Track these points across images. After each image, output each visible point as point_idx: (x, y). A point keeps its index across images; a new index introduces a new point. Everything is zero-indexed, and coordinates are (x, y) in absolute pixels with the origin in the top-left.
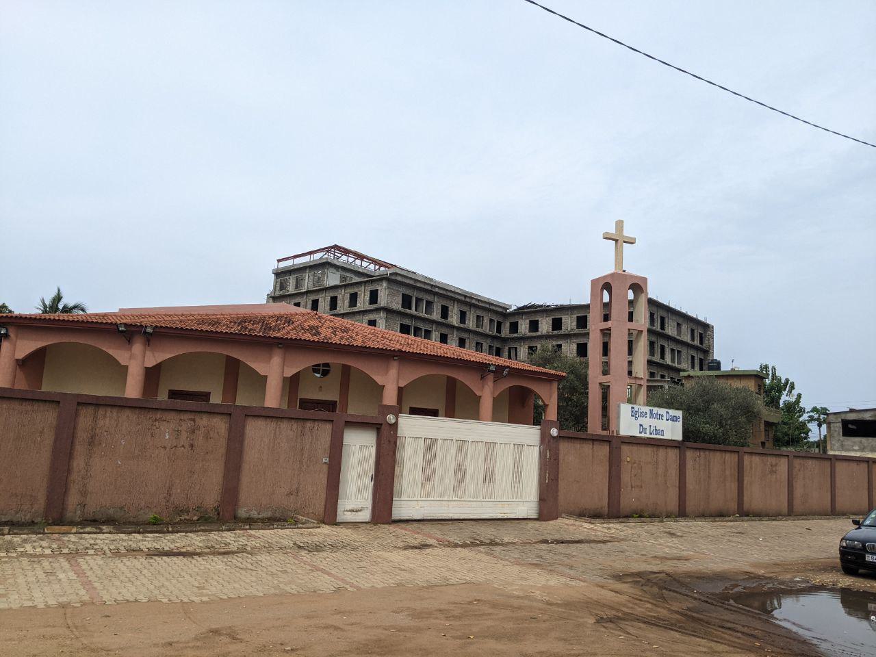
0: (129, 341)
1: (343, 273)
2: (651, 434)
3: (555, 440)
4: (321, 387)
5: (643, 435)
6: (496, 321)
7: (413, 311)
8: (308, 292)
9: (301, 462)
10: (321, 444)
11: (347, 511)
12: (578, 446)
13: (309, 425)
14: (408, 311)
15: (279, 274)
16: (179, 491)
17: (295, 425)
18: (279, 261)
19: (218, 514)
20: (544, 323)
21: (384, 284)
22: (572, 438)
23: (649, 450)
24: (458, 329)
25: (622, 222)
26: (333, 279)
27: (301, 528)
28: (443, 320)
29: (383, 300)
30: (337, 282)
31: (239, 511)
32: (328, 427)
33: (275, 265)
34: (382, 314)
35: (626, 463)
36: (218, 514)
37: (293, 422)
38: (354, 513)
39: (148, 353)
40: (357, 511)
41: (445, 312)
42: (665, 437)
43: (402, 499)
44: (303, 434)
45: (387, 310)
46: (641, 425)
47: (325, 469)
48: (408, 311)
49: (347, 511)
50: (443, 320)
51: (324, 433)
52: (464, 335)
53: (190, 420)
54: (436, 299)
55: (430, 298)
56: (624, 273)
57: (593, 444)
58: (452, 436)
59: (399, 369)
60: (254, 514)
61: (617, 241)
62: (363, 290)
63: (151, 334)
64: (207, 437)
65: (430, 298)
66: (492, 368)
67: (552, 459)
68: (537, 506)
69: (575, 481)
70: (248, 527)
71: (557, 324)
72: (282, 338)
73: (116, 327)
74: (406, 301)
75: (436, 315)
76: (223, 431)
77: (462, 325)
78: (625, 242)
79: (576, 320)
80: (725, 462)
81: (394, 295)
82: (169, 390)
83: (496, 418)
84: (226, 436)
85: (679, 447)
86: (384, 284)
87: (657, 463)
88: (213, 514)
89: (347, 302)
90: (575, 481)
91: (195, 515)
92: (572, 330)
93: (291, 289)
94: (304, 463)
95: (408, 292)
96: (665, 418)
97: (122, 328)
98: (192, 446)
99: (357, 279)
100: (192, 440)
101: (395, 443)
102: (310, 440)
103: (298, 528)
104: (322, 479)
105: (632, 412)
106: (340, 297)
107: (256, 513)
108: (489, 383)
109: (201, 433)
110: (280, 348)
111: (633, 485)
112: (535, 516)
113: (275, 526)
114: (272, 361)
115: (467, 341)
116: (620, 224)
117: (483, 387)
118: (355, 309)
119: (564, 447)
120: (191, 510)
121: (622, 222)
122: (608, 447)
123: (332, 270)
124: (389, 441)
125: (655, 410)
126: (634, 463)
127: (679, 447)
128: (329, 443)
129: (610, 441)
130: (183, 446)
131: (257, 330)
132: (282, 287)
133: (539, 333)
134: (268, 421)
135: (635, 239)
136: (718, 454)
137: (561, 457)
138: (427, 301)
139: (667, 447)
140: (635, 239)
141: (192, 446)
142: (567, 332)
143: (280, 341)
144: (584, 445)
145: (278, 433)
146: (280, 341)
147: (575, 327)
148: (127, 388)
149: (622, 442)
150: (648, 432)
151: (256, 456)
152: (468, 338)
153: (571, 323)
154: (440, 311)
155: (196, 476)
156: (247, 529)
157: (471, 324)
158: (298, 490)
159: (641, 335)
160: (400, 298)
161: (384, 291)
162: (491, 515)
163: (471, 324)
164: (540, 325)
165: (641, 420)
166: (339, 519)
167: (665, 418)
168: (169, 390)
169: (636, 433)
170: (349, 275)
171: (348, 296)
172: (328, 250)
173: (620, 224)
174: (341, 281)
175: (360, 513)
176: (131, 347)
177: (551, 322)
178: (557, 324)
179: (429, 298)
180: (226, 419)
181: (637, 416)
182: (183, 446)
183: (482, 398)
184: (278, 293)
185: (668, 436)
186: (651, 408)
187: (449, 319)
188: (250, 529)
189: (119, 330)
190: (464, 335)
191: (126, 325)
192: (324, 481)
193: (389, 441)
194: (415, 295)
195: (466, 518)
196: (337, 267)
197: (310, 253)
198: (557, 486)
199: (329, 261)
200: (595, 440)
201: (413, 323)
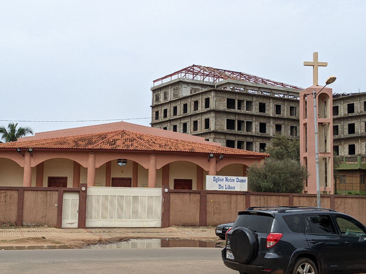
0: (24, 156)
1: (192, 87)
2: (226, 189)
3: (167, 194)
4: (122, 171)
5: (221, 189)
6: (245, 122)
7: (236, 110)
8: (170, 102)
9: (46, 206)
10: (54, 199)
11: (67, 224)
12: (181, 196)
13: (49, 192)
14: (232, 110)
15: (155, 90)
16: (2, 216)
17: (43, 193)
18: (154, 81)
19: (16, 224)
20: (342, 108)
21: (213, 94)
22: (177, 192)
23: (225, 196)
24: (274, 118)
25: (317, 53)
26: (185, 91)
27: (41, 228)
28: (262, 114)
29: (212, 105)
30: (189, 94)
31: (24, 223)
32: (57, 193)
33: (152, 85)
34: (212, 114)
35: (210, 203)
36: (16, 224)
37: (42, 192)
38: (70, 225)
39: (32, 161)
40: (72, 224)
41: (262, 108)
42: (236, 190)
43: (92, 219)
44: (46, 196)
45: (217, 112)
46: (219, 185)
47: (56, 208)
48: (232, 110)
49: (67, 224)
50: (262, 114)
51: (55, 195)
52: (279, 122)
53: (4, 192)
54: (254, 99)
55: (249, 99)
56: (317, 87)
57: (190, 195)
58: (116, 194)
59: (156, 161)
60: (29, 224)
61: (313, 66)
62: (201, 99)
63: (32, 152)
64: (10, 198)
65: (249, 99)
66: (212, 155)
67: (166, 202)
68: (161, 222)
69: (180, 211)
70: (21, 227)
71: (351, 108)
72: (92, 149)
73: (16, 150)
74: (230, 103)
75: (255, 110)
76: (16, 196)
77: (277, 116)
78: (318, 66)
79: (363, 105)
80: (279, 201)
81: (221, 100)
82: (48, 177)
83: (112, 186)
84: (17, 197)
85: (245, 195)
86: (213, 94)
87: (230, 202)
88: (14, 224)
89: (193, 107)
90: (180, 211)
91: (8, 224)
92: (345, 115)
93: (162, 101)
94: (48, 206)
95: (231, 97)
96: (235, 181)
97: (19, 150)
98: (5, 201)
99: (204, 90)
100: (6, 199)
101: (86, 198)
102: (50, 198)
103: (40, 228)
104: (56, 212)
105: (214, 179)
106: (188, 104)
107: (30, 224)
108: (212, 164)
109: (8, 197)
110: (92, 154)
111: (215, 212)
112: (160, 226)
113: (31, 227)
114: (89, 161)
115: (283, 126)
116: (316, 55)
117: (209, 166)
118: (197, 112)
119: (173, 197)
120: (6, 223)
121: (317, 53)
122: (288, 198)
123: (185, 86)
124: (83, 197)
125: (229, 177)
126: (216, 203)
127: (245, 195)
128: (57, 199)
129: (200, 193)
130: (2, 202)
131: (82, 145)
132: (157, 99)
133: (339, 116)
134: (33, 191)
135: (327, 63)
136: (274, 197)
137: (171, 201)
138: (247, 102)
139: (237, 194)
140: (327, 63)
141: (5, 201)
142: (358, 114)
143: (92, 150)
144: (185, 195)
145: (37, 196)
146: (92, 150)
147: (363, 110)
148: (24, 178)
149: (207, 193)
150: (224, 188)
151: (29, 204)
152: (283, 124)
153: (360, 107)
154: (258, 107)
155: (7, 211)
156: (21, 228)
157: (285, 114)
158: (46, 216)
159: (329, 124)
160: (225, 102)
161: (212, 98)
162: (137, 226)
163: (285, 114)
164: (339, 110)
165: (219, 183)
166: (63, 226)
167: (235, 181)
168: (48, 177)
169: (217, 188)
170: (197, 87)
171: (193, 103)
172: (187, 70)
173: (316, 55)
174: (191, 93)
175: (73, 225)
176: (25, 158)
177: (347, 107)
178: (351, 108)
179: (249, 99)
180: (17, 191)
181: (217, 181)
182: (2, 202)
183: (209, 172)
184: (155, 103)
185: (237, 189)
186: (226, 177)
187: (266, 112)
188: (22, 228)
189: (17, 151)
190: (279, 122)
191: (20, 148)
192: (56, 213)
193: (83, 197)
194: (237, 98)
195: (124, 227)
196: (188, 83)
197: (171, 75)
198: (169, 213)
199: (181, 80)
200: (195, 193)
201: (237, 118)
